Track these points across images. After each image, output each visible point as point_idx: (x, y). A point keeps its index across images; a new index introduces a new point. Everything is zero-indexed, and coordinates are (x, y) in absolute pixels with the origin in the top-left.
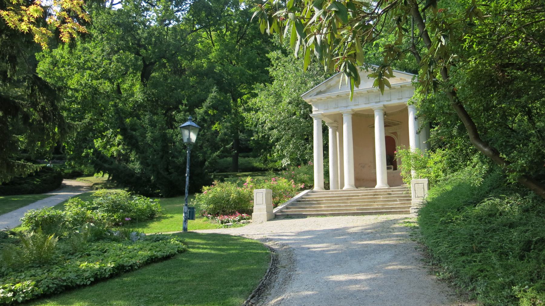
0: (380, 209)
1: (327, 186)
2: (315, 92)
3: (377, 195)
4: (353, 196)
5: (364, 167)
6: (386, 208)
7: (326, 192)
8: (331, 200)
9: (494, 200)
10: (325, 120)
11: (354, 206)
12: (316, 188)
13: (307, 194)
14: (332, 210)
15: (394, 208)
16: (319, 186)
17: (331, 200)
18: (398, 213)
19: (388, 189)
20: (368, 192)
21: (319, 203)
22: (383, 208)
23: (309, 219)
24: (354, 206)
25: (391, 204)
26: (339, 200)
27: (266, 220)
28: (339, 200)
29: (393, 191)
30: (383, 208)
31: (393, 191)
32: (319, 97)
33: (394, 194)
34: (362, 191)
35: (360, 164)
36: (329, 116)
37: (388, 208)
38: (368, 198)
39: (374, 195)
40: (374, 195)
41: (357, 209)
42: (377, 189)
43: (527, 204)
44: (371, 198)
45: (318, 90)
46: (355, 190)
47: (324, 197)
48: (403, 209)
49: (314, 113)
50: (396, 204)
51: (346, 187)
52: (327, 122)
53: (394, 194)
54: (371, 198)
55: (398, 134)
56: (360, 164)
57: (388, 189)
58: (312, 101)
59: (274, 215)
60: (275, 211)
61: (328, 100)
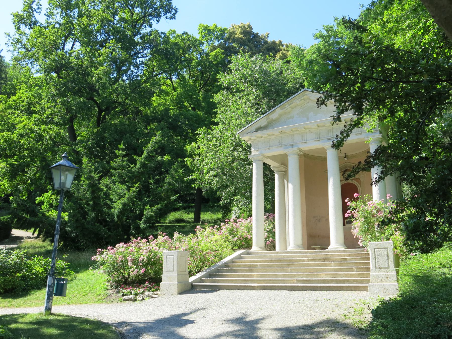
0: (328, 282)
1: (270, 246)
2: (254, 128)
3: (328, 260)
4: (296, 261)
5: (319, 221)
6: (337, 281)
7: (270, 255)
8: (268, 266)
9: (163, 329)
10: (268, 162)
11: (294, 276)
12: (254, 248)
13: (240, 257)
14: (264, 281)
15: (348, 281)
16: (257, 245)
17: (268, 266)
18: (353, 289)
19: (344, 251)
20: (317, 256)
21: (251, 271)
22: (332, 281)
23: (221, 292)
24: (294, 276)
25: (342, 276)
26: (278, 266)
27: (177, 293)
28: (278, 266)
29: (349, 255)
30: (332, 281)
31: (349, 255)
32: (259, 134)
33: (350, 260)
34: (312, 254)
35: (314, 217)
36: (273, 158)
37: (340, 282)
38: (242, 263)
39: (324, 260)
40: (324, 260)
41: (299, 281)
42: (328, 252)
43: (89, 125)
44: (319, 265)
45: (257, 125)
46: (300, 252)
47: (260, 262)
48: (360, 283)
49: (252, 154)
50: (352, 275)
51: (291, 247)
52: (273, 165)
53: (350, 260)
54: (319, 265)
55: (362, 180)
56: (314, 217)
57: (344, 251)
58: (251, 139)
59: (190, 286)
60: (191, 279)
61: (270, 137)
